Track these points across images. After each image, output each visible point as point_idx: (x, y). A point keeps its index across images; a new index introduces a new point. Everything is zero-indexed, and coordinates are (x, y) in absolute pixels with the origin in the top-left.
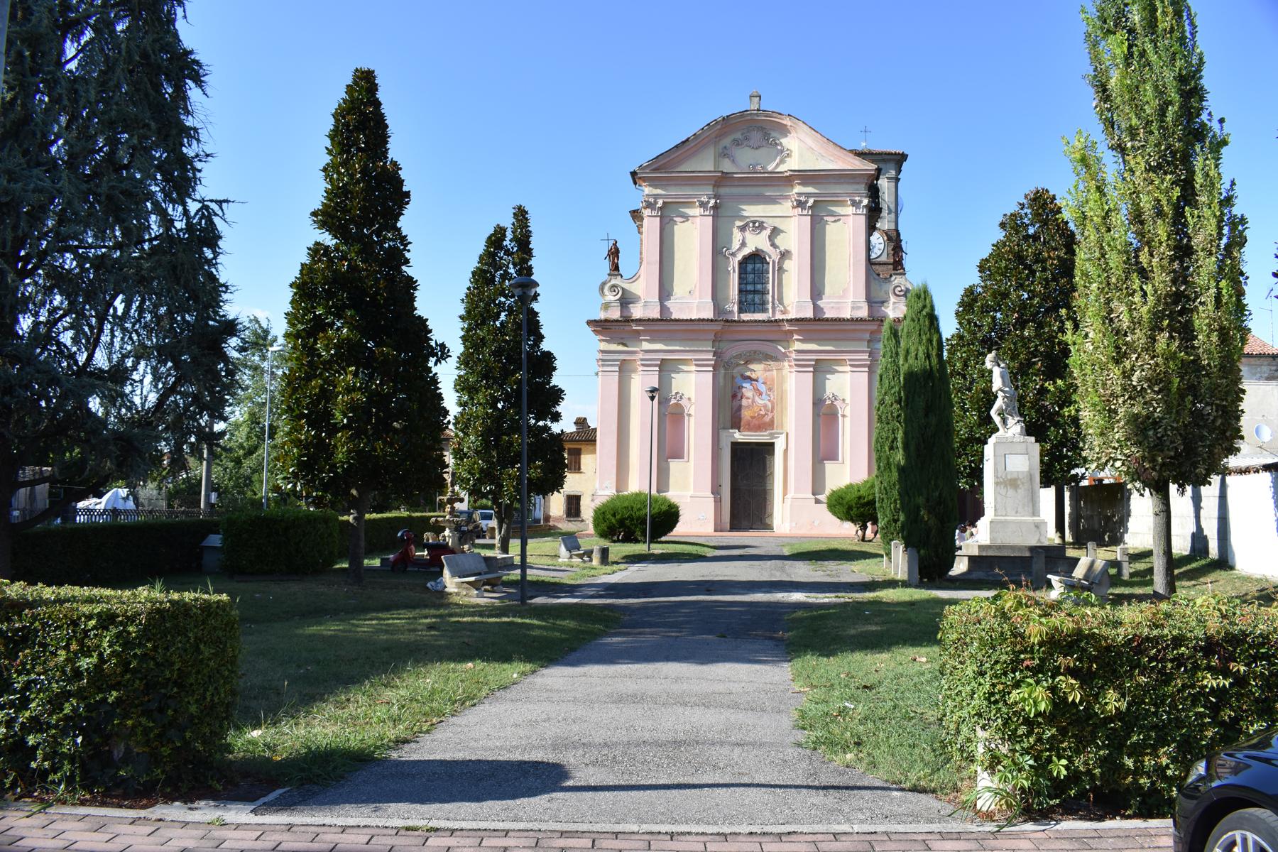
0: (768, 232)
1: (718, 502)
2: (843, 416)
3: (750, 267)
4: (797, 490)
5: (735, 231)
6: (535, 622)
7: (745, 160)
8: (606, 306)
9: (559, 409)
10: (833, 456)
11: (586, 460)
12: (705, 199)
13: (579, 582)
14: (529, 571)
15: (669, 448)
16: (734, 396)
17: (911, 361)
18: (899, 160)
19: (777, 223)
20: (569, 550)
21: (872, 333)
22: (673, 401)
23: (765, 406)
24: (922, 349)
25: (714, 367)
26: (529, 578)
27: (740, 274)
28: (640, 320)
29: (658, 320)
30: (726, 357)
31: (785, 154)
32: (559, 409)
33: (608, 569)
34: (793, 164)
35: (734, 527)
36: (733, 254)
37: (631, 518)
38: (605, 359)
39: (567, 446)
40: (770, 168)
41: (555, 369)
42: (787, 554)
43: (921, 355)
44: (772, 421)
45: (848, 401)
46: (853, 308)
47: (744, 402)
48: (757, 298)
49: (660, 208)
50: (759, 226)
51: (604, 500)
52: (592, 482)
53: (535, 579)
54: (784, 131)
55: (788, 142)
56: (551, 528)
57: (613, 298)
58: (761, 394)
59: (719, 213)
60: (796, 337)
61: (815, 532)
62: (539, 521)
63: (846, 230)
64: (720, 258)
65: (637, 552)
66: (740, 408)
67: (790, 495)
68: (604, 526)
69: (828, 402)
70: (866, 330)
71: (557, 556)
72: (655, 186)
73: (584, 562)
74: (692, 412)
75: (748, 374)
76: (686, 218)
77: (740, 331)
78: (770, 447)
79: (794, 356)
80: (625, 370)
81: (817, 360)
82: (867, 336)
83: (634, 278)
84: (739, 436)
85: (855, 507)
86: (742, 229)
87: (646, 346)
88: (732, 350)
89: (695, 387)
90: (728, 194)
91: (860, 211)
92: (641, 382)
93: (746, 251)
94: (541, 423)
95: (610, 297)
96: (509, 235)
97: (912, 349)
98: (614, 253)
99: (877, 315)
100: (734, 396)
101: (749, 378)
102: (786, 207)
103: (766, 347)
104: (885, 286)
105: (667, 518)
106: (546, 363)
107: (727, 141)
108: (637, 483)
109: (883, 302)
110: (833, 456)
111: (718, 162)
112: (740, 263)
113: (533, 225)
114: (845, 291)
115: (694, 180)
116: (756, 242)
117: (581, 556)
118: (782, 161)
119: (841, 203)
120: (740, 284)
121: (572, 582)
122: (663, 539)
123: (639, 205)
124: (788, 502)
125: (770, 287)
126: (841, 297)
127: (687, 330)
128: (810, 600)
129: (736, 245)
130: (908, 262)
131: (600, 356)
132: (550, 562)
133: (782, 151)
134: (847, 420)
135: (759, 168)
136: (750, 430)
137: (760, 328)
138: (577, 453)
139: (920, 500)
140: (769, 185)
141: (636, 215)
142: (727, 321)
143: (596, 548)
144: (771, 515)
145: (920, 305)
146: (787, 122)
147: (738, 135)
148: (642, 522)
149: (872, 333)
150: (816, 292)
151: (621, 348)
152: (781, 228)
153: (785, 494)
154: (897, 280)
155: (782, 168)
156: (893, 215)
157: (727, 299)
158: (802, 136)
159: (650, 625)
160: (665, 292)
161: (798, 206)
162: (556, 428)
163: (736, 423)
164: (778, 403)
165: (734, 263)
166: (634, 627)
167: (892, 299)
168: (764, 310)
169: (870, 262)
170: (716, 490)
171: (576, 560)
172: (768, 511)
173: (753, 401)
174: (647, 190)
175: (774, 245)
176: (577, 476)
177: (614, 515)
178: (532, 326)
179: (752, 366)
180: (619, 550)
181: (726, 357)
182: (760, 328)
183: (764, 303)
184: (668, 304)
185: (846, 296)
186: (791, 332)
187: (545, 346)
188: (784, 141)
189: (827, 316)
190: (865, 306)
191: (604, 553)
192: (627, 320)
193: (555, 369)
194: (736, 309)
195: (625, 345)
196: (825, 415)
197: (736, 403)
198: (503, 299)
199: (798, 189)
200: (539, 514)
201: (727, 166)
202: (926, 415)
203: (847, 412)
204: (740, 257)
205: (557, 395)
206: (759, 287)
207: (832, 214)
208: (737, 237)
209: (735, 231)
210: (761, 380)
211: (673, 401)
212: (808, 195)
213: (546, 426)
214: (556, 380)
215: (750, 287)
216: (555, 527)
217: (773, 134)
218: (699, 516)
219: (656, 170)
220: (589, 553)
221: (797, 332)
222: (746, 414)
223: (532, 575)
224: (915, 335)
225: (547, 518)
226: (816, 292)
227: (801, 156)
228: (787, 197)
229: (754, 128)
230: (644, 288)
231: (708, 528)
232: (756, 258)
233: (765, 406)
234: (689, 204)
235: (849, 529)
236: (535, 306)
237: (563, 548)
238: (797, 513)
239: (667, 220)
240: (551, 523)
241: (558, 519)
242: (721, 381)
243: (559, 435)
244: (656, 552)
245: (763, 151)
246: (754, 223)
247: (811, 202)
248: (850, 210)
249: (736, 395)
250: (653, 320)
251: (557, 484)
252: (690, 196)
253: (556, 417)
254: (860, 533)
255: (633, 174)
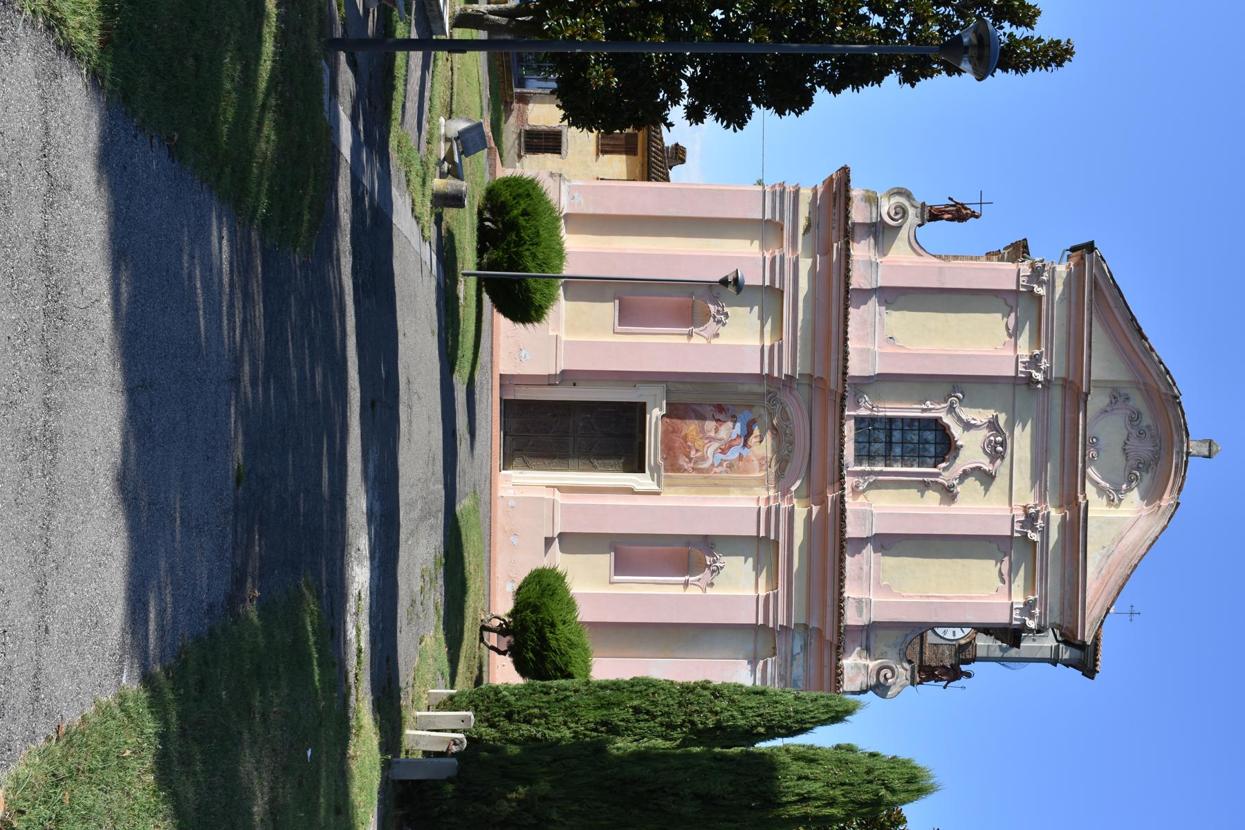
0: (987, 466)
1: (549, 381)
2: (686, 584)
3: (930, 436)
4: (567, 508)
5: (989, 414)
6: (266, 67)
7: (1107, 430)
8: (872, 200)
9: (710, 119)
10: (621, 567)
11: (617, 164)
12: (1044, 364)
13: (393, 155)
14: (417, 57)
15: (637, 300)
16: (720, 408)
17: (796, 767)
18: (1085, 659)
19: (1001, 482)
20: (461, 135)
21: (820, 632)
22: (713, 308)
23: (703, 458)
24: (817, 787)
25: (769, 376)
26: (400, 56)
27: (919, 420)
28: (848, 256)
29: (847, 284)
30: (784, 396)
31: (1114, 495)
32: (710, 119)
33: (426, 209)
34: (1097, 508)
35: (510, 408)
36: (951, 410)
37: (520, 242)
38: (784, 197)
39: (641, 135)
40: (1091, 471)
41: (781, 112)
42: (458, 508)
43: (807, 786)
44: (680, 469)
45: (710, 591)
46: (859, 601)
47: (710, 425)
48: (879, 447)
49: (1031, 291)
50: (996, 451)
51: (552, 196)
52: (580, 175)
53: (399, 72)
54: (1152, 496)
55: (1132, 504)
56: (508, 105)
57: (884, 210)
58: (723, 451)
59: (1016, 390)
60: (815, 509)
61: (499, 537)
62: (521, 84)
63: (982, 592)
64: (947, 388)
65: (459, 254)
66: (701, 417)
67: (558, 496)
68: (506, 195)
69: (709, 560)
70: (824, 623)
71: (450, 115)
72: (1067, 283)
73: (440, 163)
74: (696, 340)
75: (756, 431)
76: (1014, 334)
77: (825, 419)
78: (636, 464)
79: (785, 505)
80: (766, 229)
81: (776, 542)
82: (814, 624)
83: (917, 246)
84: (655, 414)
85: (538, 628)
86: (993, 425)
87: (805, 265)
88: (795, 406)
89: (736, 344)
90: (1050, 402)
91: (1016, 615)
92: (743, 256)
93: (956, 431)
94: (685, 87)
95: (886, 206)
96: (1020, 32)
97: (817, 771)
98: (959, 213)
99: (847, 639)
100: (720, 408)
101: (749, 434)
102: (1025, 495)
103: (798, 460)
104: (893, 652)
105: (522, 305)
106: (792, 99)
107: (1138, 401)
108: (580, 251)
109: (868, 649)
110: (621, 567)
111: (1102, 387)
112: (937, 421)
113: (1036, 77)
114: (888, 589)
115: (1076, 346)
116: (972, 447)
117: (449, 157)
118: (1101, 491)
119: (1030, 585)
120: (903, 419)
121: (393, 143)
122: (486, 298)
123: (1036, 254)
124: (548, 495)
125: (897, 468)
126: (878, 583)
127: (830, 335)
128: (351, 605)
129: (967, 414)
130: (932, 689)
131: (789, 188)
132: (437, 103)
133: (1118, 491)
134: (679, 590)
135: (1092, 452)
136: (666, 433)
137: (830, 451)
138: (628, 149)
139: (544, 787)
140: (1063, 473)
141: (1019, 250)
142: (843, 398)
143: (463, 185)
144: (528, 466)
145: (897, 785)
146: (1167, 500)
147: (1147, 420)
148: (512, 258)
149: (820, 632)
150: (887, 543)
151: (802, 223)
152: (993, 488)
153: (561, 489)
154: (903, 671)
155: (1090, 490)
156: (998, 654)
157: (878, 397)
158: (1142, 524)
159: (274, 317)
160: (894, 297)
161: (1027, 515)
162: (677, 113)
163: (676, 411)
164: (709, 480)
165: (938, 410)
166: (268, 282)
167: (873, 664)
168: (859, 459)
169: (932, 626)
170: (568, 377)
171: (442, 150)
172: (533, 462)
173: (711, 439)
174: (1062, 269)
175: (965, 475)
176: (592, 147)
177: (525, 213)
178: (858, 72)
179: (768, 437)
180: (465, 226)
181: (784, 396)
182: (830, 451)
183: (871, 458)
184: (873, 301)
185: (878, 590)
186: (822, 502)
187: (821, 95)
188: (1135, 495)
189: (849, 560)
190: (863, 621)
191: (456, 200)
192: (848, 234)
193: (781, 112)
194: (863, 412)
195: (807, 230)
196: (689, 554)
197: (709, 411)
198: (907, 20)
199: (1055, 515)
200: (533, 86)
201: (1097, 401)
202: (696, 796)
203: (693, 591)
204: (947, 420)
205: (735, 117)
206: (897, 450)
207: (1013, 571)
208: (980, 416)
209: (989, 414)
210: (745, 452)
211: (713, 308)
212: (1045, 533)
213: (681, 96)
214: (761, 116)
215: (897, 435)
216: (509, 111)
217: (1147, 478)
218: (520, 352)
219: (1095, 284)
220: (456, 172)
221: (823, 511)
222: (691, 427)
223: (409, 64)
224: (842, 776)
225: (524, 99)
226: (887, 543)
227: (1110, 522)
228: (1042, 498)
229: (1159, 445)
230: (901, 263)
231: (505, 365)
232: (946, 447)
233: (703, 458)
234: (1036, 339)
235: (503, 605)
236: (892, 79)
237: (462, 125)
238: (531, 511)
239: (1011, 301)
240: (515, 105)
241: (522, 117)
242: (746, 388)
243: (664, 120)
244: (461, 289)
245: (1118, 459)
246: (1003, 444)
247: (1035, 537)
248: (1019, 599)
249: (722, 412)
250: (847, 277)
251: (578, 116)
252: (1050, 341)
253: (695, 115)
254: (496, 623)
255: (1090, 247)
